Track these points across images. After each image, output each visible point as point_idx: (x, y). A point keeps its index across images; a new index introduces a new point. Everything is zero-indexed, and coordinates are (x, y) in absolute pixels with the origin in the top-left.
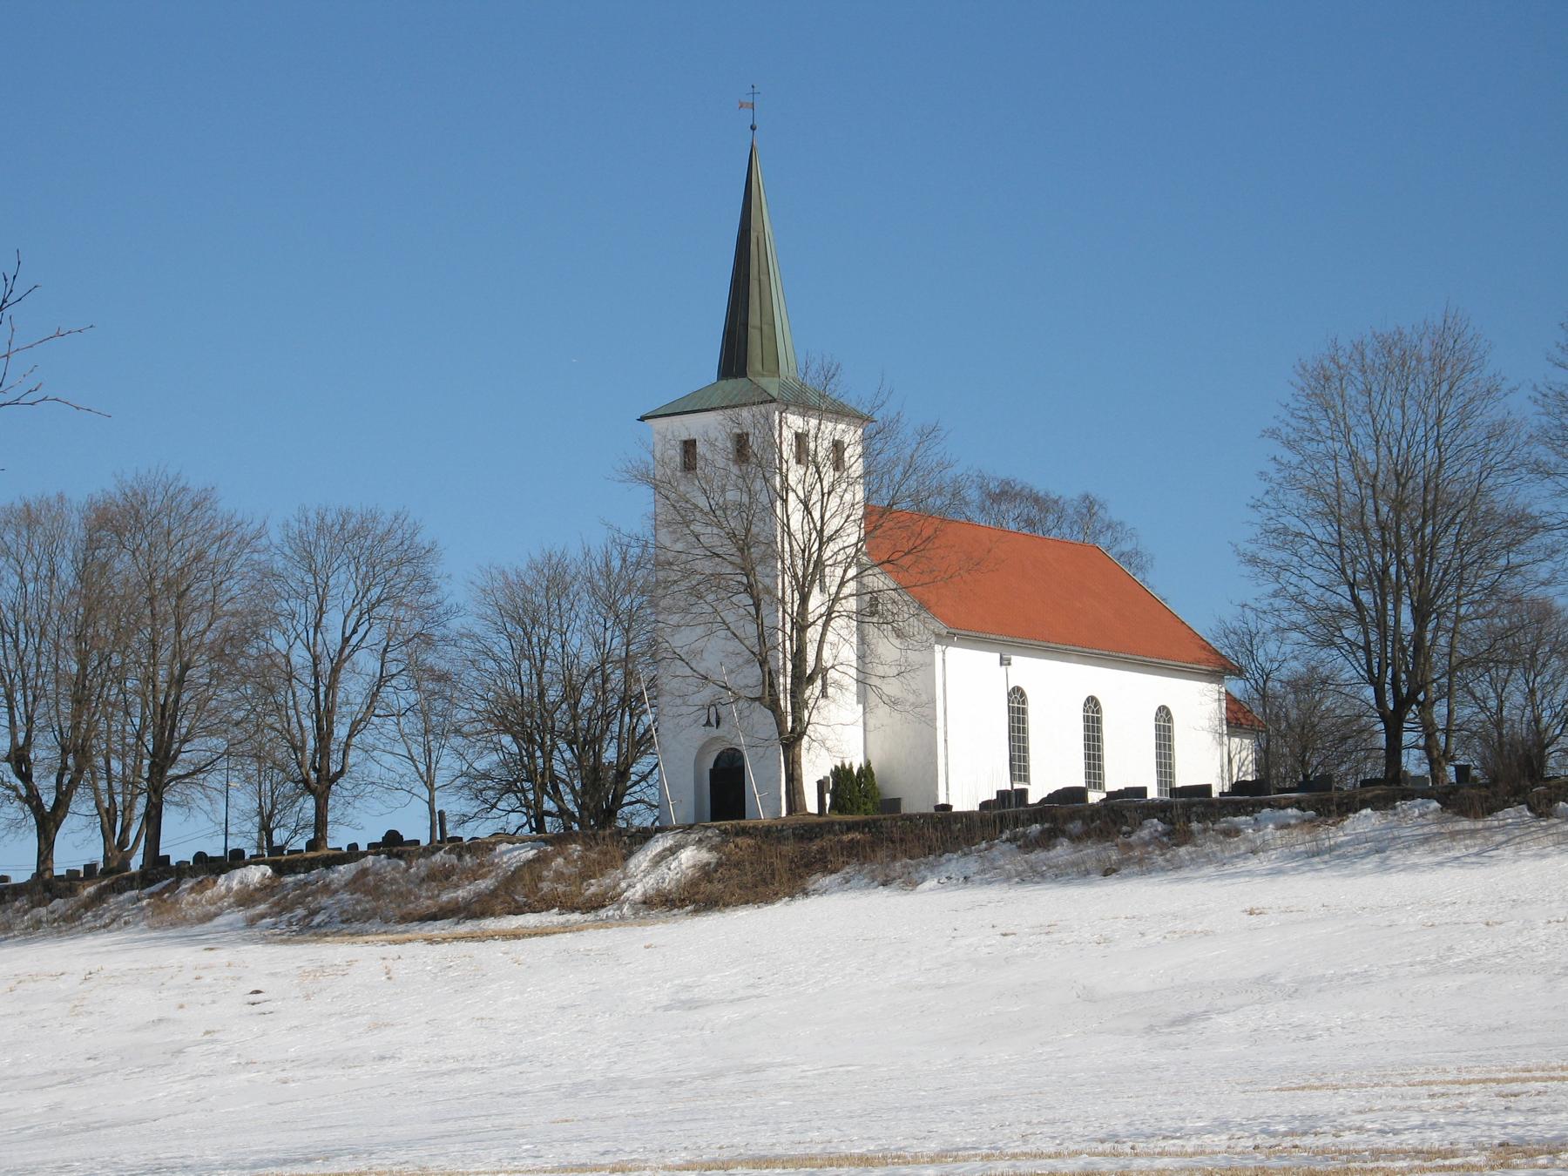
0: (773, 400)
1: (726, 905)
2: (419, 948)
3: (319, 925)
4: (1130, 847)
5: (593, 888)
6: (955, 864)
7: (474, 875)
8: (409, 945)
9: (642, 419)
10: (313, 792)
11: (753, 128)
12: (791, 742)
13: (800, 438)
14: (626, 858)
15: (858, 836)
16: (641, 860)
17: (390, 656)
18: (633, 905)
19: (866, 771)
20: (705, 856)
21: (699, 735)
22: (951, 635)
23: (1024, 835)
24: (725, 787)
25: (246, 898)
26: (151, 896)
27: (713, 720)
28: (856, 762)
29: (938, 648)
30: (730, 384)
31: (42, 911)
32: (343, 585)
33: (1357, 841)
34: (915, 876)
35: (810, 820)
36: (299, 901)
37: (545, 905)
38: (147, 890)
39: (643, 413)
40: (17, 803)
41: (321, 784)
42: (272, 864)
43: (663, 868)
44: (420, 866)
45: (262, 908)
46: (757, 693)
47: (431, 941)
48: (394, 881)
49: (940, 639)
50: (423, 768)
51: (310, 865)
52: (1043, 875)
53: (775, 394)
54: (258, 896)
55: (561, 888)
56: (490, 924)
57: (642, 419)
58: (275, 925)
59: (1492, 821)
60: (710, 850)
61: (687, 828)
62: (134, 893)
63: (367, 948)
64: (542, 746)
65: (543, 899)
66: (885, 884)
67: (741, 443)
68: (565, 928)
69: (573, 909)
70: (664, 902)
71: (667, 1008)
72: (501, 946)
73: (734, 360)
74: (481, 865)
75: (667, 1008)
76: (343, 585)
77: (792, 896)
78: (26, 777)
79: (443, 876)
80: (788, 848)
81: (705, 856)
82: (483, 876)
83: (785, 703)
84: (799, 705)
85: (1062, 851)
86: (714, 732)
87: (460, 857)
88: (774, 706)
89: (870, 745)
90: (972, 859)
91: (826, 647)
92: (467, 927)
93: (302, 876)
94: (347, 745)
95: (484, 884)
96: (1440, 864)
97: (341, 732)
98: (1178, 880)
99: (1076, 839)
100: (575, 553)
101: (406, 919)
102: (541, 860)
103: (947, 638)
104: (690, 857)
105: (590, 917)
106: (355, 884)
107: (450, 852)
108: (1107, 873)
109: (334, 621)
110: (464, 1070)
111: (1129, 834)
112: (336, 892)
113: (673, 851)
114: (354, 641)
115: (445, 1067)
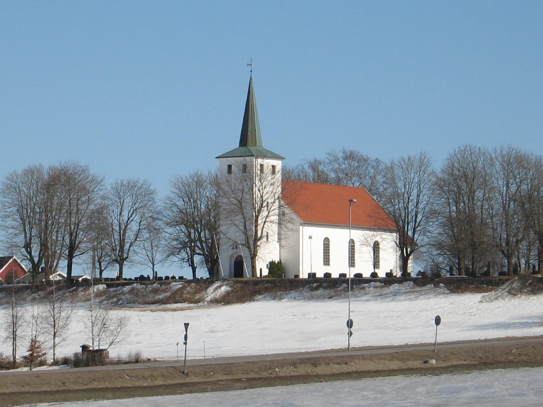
0: (253, 156)
1: (232, 303)
2: (148, 313)
3: (120, 304)
4: (337, 291)
5: (197, 297)
6: (293, 293)
7: (164, 291)
8: (146, 312)
9: (217, 158)
10: (119, 263)
11: (251, 71)
12: (253, 256)
13: (262, 166)
14: (207, 288)
15: (270, 285)
16: (211, 289)
17: (142, 223)
18: (208, 302)
19: (280, 262)
20: (228, 289)
21: (231, 252)
22: (305, 224)
23: (312, 286)
24: (238, 267)
25: (99, 294)
26: (69, 292)
27: (235, 247)
28: (277, 260)
29: (301, 227)
30: (243, 149)
31: (35, 295)
32: (128, 202)
33: (391, 293)
34: (282, 297)
35: (257, 279)
36: (114, 297)
37: (184, 301)
38: (69, 290)
39: (217, 156)
40: (28, 261)
41: (121, 261)
42: (107, 284)
43: (216, 292)
44: (150, 288)
45: (104, 298)
46: (244, 242)
47: (152, 311)
48: (142, 292)
49: (301, 224)
50: (151, 258)
51: (118, 285)
52: (314, 298)
53: (254, 153)
54: (102, 294)
55: (188, 296)
56: (169, 306)
57: (217, 158)
58: (108, 303)
59: (423, 288)
60: (230, 287)
61: (224, 280)
62: (64, 291)
63: (134, 312)
64: (198, 230)
65: (183, 300)
66: (274, 299)
67: (245, 167)
68: (189, 308)
69: (191, 303)
70: (216, 302)
71: (207, 332)
72: (170, 313)
73: (244, 141)
74: (167, 288)
75: (207, 332)
76: (128, 202)
77: (250, 301)
78: (30, 253)
79: (155, 291)
80: (251, 287)
81: (228, 289)
82: (167, 292)
83: (252, 247)
84: (256, 246)
85: (320, 292)
86: (235, 250)
87: (161, 285)
88: (249, 247)
89: (281, 255)
90: (297, 293)
91: (264, 229)
92: (161, 307)
93: (115, 288)
94: (129, 250)
95: (168, 294)
96: (405, 300)
97: (127, 246)
98: (343, 302)
99: (325, 288)
100: (205, 173)
101: (145, 303)
102: (184, 288)
103: (304, 224)
104: (224, 289)
105: (196, 305)
106: (131, 292)
107: (158, 284)
108: (330, 298)
109: (125, 214)
110: (157, 346)
111: (338, 287)
112: (125, 294)
113: (220, 287)
114: (131, 219)
115: (153, 345)
